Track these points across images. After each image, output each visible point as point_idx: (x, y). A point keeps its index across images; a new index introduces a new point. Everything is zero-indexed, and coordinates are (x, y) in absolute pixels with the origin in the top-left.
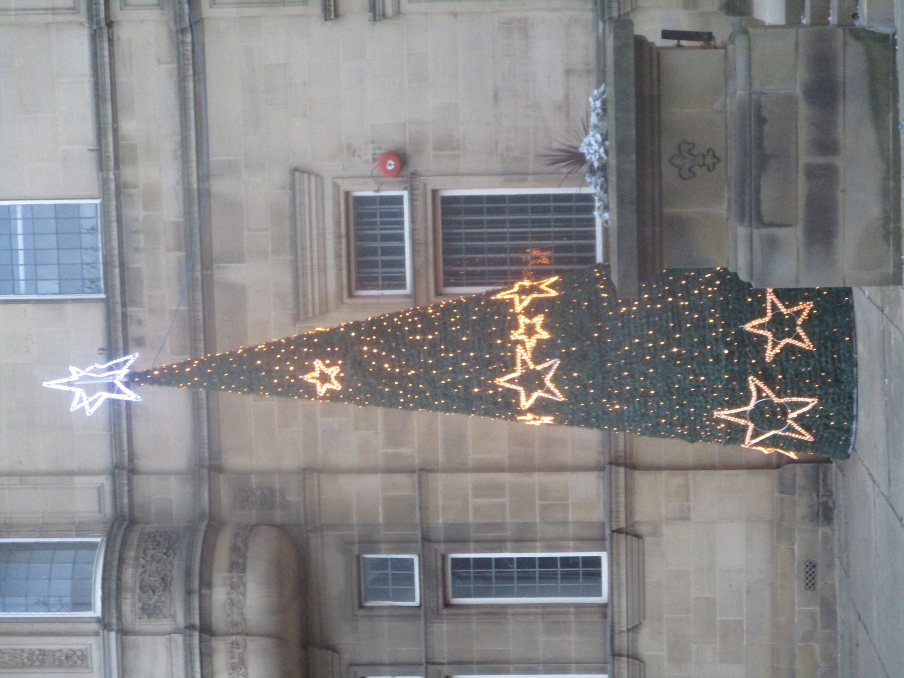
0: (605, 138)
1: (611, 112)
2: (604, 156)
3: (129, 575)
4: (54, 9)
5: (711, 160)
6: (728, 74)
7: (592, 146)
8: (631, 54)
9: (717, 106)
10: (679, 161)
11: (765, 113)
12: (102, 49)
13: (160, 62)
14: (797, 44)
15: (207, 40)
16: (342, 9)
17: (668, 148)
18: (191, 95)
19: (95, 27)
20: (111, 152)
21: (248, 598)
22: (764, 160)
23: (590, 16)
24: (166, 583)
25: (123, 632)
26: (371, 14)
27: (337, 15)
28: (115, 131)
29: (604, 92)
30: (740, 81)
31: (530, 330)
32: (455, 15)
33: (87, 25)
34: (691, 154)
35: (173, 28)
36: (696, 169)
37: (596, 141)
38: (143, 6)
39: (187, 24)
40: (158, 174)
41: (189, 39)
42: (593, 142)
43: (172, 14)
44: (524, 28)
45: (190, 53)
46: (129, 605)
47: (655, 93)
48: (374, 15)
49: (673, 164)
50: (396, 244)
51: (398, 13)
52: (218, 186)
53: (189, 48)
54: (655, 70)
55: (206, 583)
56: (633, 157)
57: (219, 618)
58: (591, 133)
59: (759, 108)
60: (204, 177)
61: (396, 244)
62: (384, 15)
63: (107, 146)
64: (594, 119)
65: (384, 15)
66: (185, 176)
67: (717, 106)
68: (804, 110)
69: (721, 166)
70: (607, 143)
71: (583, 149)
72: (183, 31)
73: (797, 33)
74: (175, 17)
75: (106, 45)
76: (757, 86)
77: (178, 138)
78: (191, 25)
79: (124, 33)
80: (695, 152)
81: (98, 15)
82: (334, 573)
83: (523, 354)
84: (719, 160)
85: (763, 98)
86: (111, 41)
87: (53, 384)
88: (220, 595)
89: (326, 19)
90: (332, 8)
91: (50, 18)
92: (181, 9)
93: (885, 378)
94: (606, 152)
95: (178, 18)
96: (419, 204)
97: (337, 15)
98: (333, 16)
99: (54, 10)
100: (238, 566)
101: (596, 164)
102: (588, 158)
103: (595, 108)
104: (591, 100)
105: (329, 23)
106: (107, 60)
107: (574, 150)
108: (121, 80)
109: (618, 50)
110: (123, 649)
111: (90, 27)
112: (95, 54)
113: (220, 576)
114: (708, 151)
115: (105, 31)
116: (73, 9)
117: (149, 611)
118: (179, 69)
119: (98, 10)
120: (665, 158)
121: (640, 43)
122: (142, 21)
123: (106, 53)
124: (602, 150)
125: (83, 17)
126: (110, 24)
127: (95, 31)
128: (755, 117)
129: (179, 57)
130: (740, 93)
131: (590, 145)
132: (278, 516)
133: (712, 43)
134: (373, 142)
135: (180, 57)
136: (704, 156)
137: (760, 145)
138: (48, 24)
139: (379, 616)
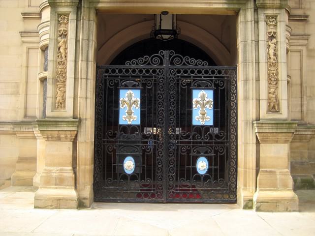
51: (24, 42)
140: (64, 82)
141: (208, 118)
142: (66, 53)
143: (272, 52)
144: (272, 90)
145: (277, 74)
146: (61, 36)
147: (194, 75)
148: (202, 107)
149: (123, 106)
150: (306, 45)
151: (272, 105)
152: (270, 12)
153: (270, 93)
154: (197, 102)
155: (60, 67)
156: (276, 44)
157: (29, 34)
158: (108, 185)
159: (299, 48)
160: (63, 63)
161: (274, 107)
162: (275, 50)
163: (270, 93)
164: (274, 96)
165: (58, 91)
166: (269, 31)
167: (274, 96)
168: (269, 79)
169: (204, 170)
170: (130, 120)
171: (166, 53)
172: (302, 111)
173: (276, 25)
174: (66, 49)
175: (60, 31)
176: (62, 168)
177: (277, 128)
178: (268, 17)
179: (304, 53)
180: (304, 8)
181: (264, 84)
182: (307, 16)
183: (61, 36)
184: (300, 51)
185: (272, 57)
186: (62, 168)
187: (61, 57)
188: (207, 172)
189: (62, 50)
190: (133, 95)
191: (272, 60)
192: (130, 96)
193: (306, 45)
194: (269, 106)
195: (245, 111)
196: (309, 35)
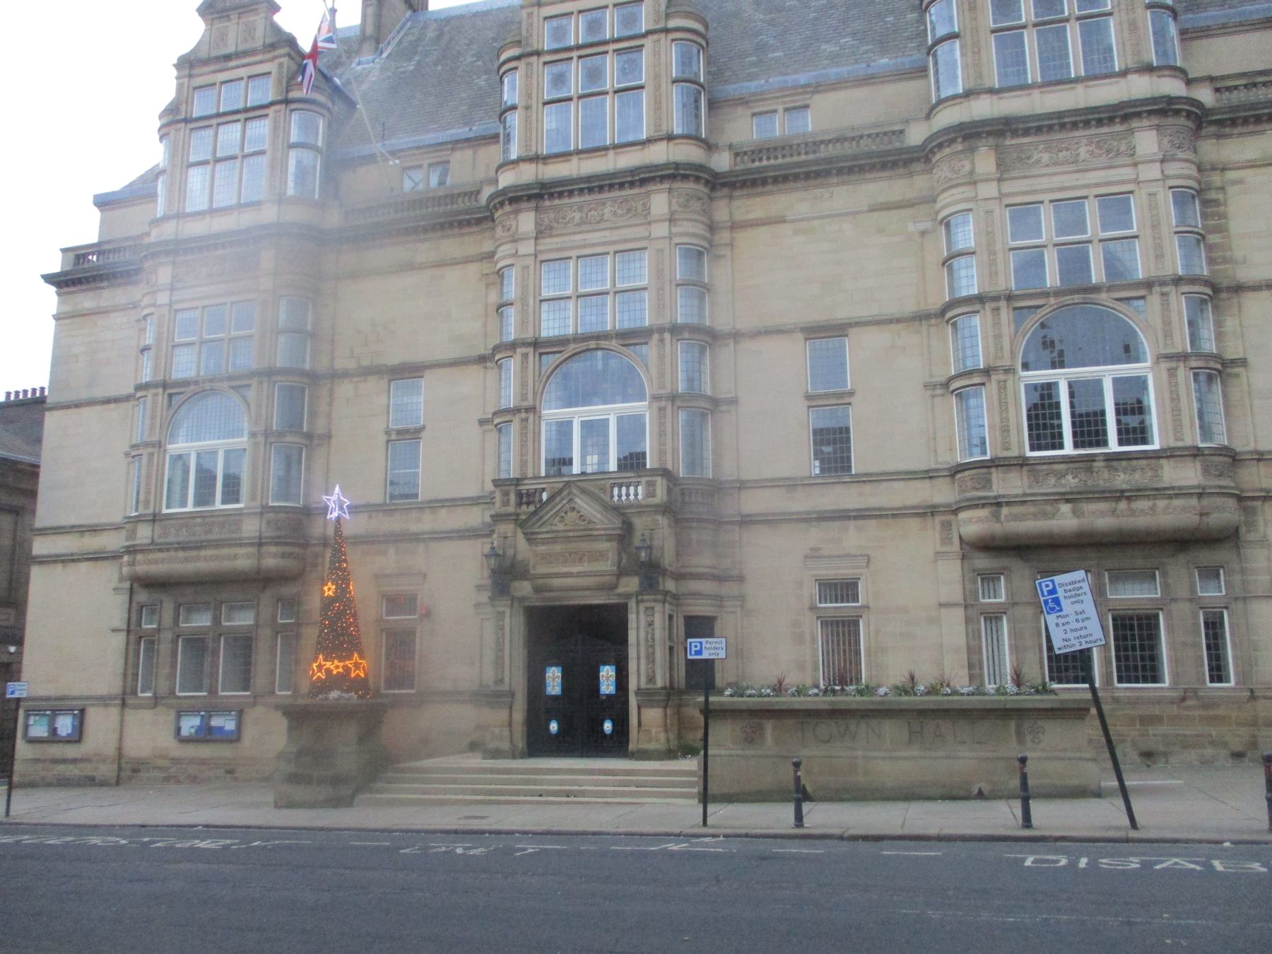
3: (282, 516)
20: (435, 505)
21: (272, 560)
24: (278, 529)
25: (262, 514)
31: (337, 667)
40: (427, 523)
46: (271, 515)
52: (421, 547)
55: (277, 544)
57: (264, 549)
60: (424, 540)
66: (424, 533)
82: (289, 590)
83: (328, 664)
87: (337, 489)
88: (273, 549)
93: (1232, 843)
100: (283, 556)
110: (255, 514)
113: (279, 549)
117: (268, 523)
125: (933, 466)
132: (308, 569)
139: (929, 475)
150: (742, 606)
152: (648, 604)
158: (538, 744)
168: (648, 658)
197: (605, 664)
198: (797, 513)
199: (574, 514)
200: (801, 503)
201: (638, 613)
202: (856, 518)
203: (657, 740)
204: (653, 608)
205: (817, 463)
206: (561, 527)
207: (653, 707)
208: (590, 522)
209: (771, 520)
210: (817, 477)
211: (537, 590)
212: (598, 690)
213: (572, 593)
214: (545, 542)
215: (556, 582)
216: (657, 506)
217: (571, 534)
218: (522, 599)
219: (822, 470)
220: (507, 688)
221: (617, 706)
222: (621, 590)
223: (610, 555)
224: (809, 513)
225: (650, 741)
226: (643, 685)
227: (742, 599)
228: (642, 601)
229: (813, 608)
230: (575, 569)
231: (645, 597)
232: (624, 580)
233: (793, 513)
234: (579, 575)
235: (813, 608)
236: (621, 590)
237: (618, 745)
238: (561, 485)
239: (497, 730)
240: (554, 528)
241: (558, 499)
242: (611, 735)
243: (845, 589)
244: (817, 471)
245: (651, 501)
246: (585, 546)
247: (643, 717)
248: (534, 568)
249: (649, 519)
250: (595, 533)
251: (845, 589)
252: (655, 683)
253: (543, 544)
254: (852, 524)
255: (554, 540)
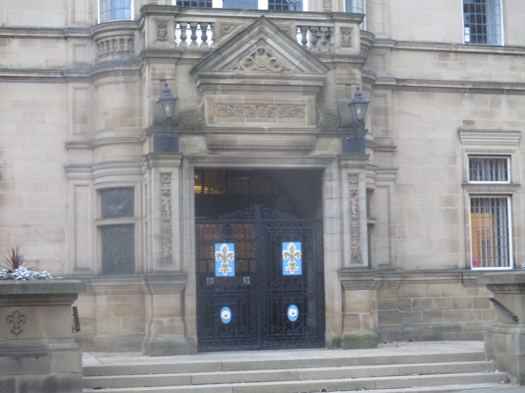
0: (27, 279)
1: (38, 282)
2: (18, 278)
4: (74, 11)
5: (17, 331)
6: (60, 339)
7: (22, 272)
8: (71, 291)
9: (44, 334)
10: (16, 315)
11: (41, 358)
12: (54, 33)
13: (47, 61)
14: (75, 373)
15: (57, 85)
16: (71, 151)
17: (23, 310)
18: (30, 75)
19: (65, 31)
22: (18, 358)
23: (66, 272)
26: (68, 165)
27: (68, 149)
28: (13, 37)
29: (48, 278)
30: (57, 345)
32: (67, 206)
33: (66, 27)
34: (20, 322)
35: (64, 69)
36: (12, 324)
37: (25, 274)
38: (74, 55)
39: (66, 75)
41: (58, 76)
42: (24, 272)
43: (70, 68)
44: (60, 240)
45: (51, 76)
47: (51, 303)
48: (68, 167)
49: (15, 312)
50: (494, 177)
51: (69, 179)
53: (54, 76)
54: (64, 303)
56: (20, 293)
58: (29, 272)
59: (44, 355)
61: (478, 177)
62: (67, 172)
63: (6, 32)
64: (36, 273)
65: (68, 172)
67: (44, 334)
68: (43, 377)
69: (13, 336)
70: (24, 280)
71: (21, 268)
72: (62, 73)
73: (81, 373)
74: (68, 70)
75: (56, 35)
76: (54, 353)
77: (9, 68)
78: (65, 77)
79: (61, 45)
80: (21, 323)
81: (71, 32)
84: (17, 335)
85: (49, 356)
86: (58, 38)
89: (66, 143)
90: (72, 147)
91: (70, 9)
92: (73, 73)
94: (20, 279)
95: (69, 71)
96: (504, 188)
97: (68, 149)
98: (68, 147)
99: (74, 12)
101: (13, 274)
102: (16, 270)
103: (41, 274)
104: (45, 272)
105: (64, 145)
106: (48, 35)
107: (20, 263)
108: (39, 42)
109: (73, 284)
111: (66, 29)
112: (52, 30)
114: (22, 330)
115: (63, 35)
116: (74, 21)
118: (44, 70)
119: (73, 33)
120: (17, 308)
121: (74, 296)
122: (67, 54)
123: (52, 35)
124: (21, 277)
125: (70, 25)
126: (66, 38)
127: (63, 30)
128: (40, 353)
129: (48, 70)
130: (51, 345)
131: (23, 271)
133: (75, 331)
134: (4, 164)
135: (49, 71)
136: (18, 328)
137: (27, 356)
138: (67, 8)
139: (64, 34)
140: (170, 238)
141: (297, 269)
142: (170, 212)
143: (354, 208)
144: (355, 243)
145: (359, 228)
146: (164, 195)
147: (283, 228)
148: (292, 258)
149: (218, 259)
150: (394, 180)
151: (355, 256)
152: (351, 171)
153: (352, 245)
154: (287, 254)
155: (166, 224)
156: (357, 201)
157: (77, 169)
158: (211, 336)
159: (387, 183)
160: (168, 221)
161: (356, 257)
162: (357, 206)
163: (352, 245)
164: (356, 248)
165: (164, 246)
166: (352, 188)
167: (356, 248)
168: (352, 233)
169: (295, 317)
170: (225, 272)
171: (257, 207)
172: (390, 256)
173: (357, 183)
174: (170, 207)
175: (163, 190)
176: (172, 318)
177: (356, 276)
178: (350, 175)
179: (392, 188)
180: (391, 138)
181: (347, 238)
182: (394, 147)
183: (164, 195)
184: (387, 187)
185: (354, 212)
186: (172, 318)
187: (166, 215)
188: (297, 319)
189: (166, 208)
190: (228, 248)
191: (354, 216)
192: (224, 250)
193: (394, 180)
194: (352, 257)
195: (332, 263)
196: (397, 169)
197: (288, 240)
198: (452, 82)
199: (264, 57)
200: (453, 71)
201: (340, 180)
202: (509, 92)
203: (367, 326)
204: (356, 175)
205: (468, 30)
206: (248, 72)
207: (358, 288)
208: (284, 69)
209: (426, 88)
210: (467, 44)
211: (213, 148)
212: (281, 270)
213: (257, 154)
214: (227, 89)
215: (240, 139)
216: (354, 57)
217: (263, 82)
218: (193, 159)
219: (473, 39)
220: (177, 268)
221: (308, 288)
222: (317, 153)
223: (306, 110)
224: (462, 83)
225: (358, 326)
226: (347, 264)
227: (394, 170)
228: (346, 167)
229: (465, 185)
230: (266, 125)
231: (350, 162)
232: (323, 141)
233: (444, 82)
234: (271, 132)
235: (465, 185)
236: (317, 153)
237: (309, 333)
238: (248, 23)
239: (165, 321)
240: (242, 73)
241: (246, 37)
242: (297, 323)
243: (496, 164)
244: (468, 39)
245: (345, 51)
246: (276, 97)
247: (347, 300)
248: (211, 119)
249: (344, 72)
250: (292, 82)
251: (496, 164)
252: (360, 262)
253: (223, 91)
254: (504, 98)
255: (238, 88)
